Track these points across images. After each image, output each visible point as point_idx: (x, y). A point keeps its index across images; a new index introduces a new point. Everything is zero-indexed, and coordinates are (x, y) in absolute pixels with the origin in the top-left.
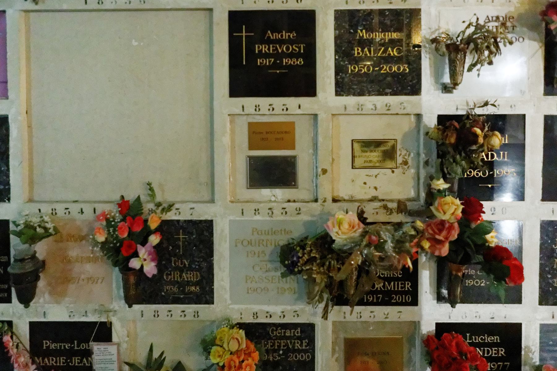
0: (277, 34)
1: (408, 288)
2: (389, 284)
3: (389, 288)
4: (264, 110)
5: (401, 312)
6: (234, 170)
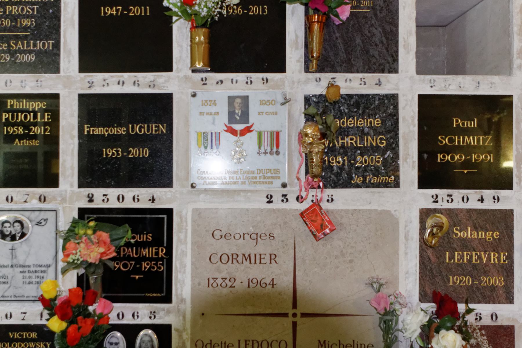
1: (15, 11)
6: (295, 140)
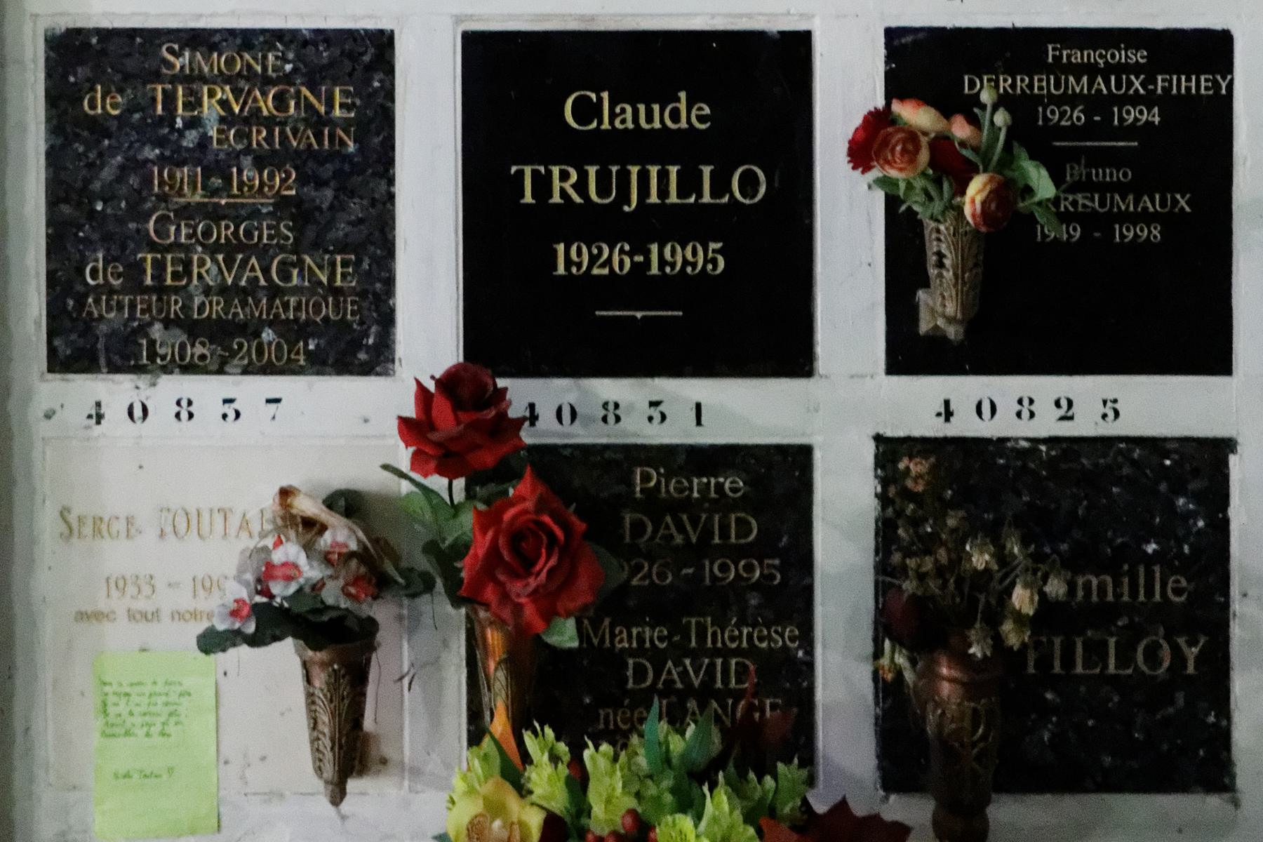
0: (1109, 579)
2: (1078, 81)
3: (596, 641)
4: (1007, 408)
5: (277, 401)
